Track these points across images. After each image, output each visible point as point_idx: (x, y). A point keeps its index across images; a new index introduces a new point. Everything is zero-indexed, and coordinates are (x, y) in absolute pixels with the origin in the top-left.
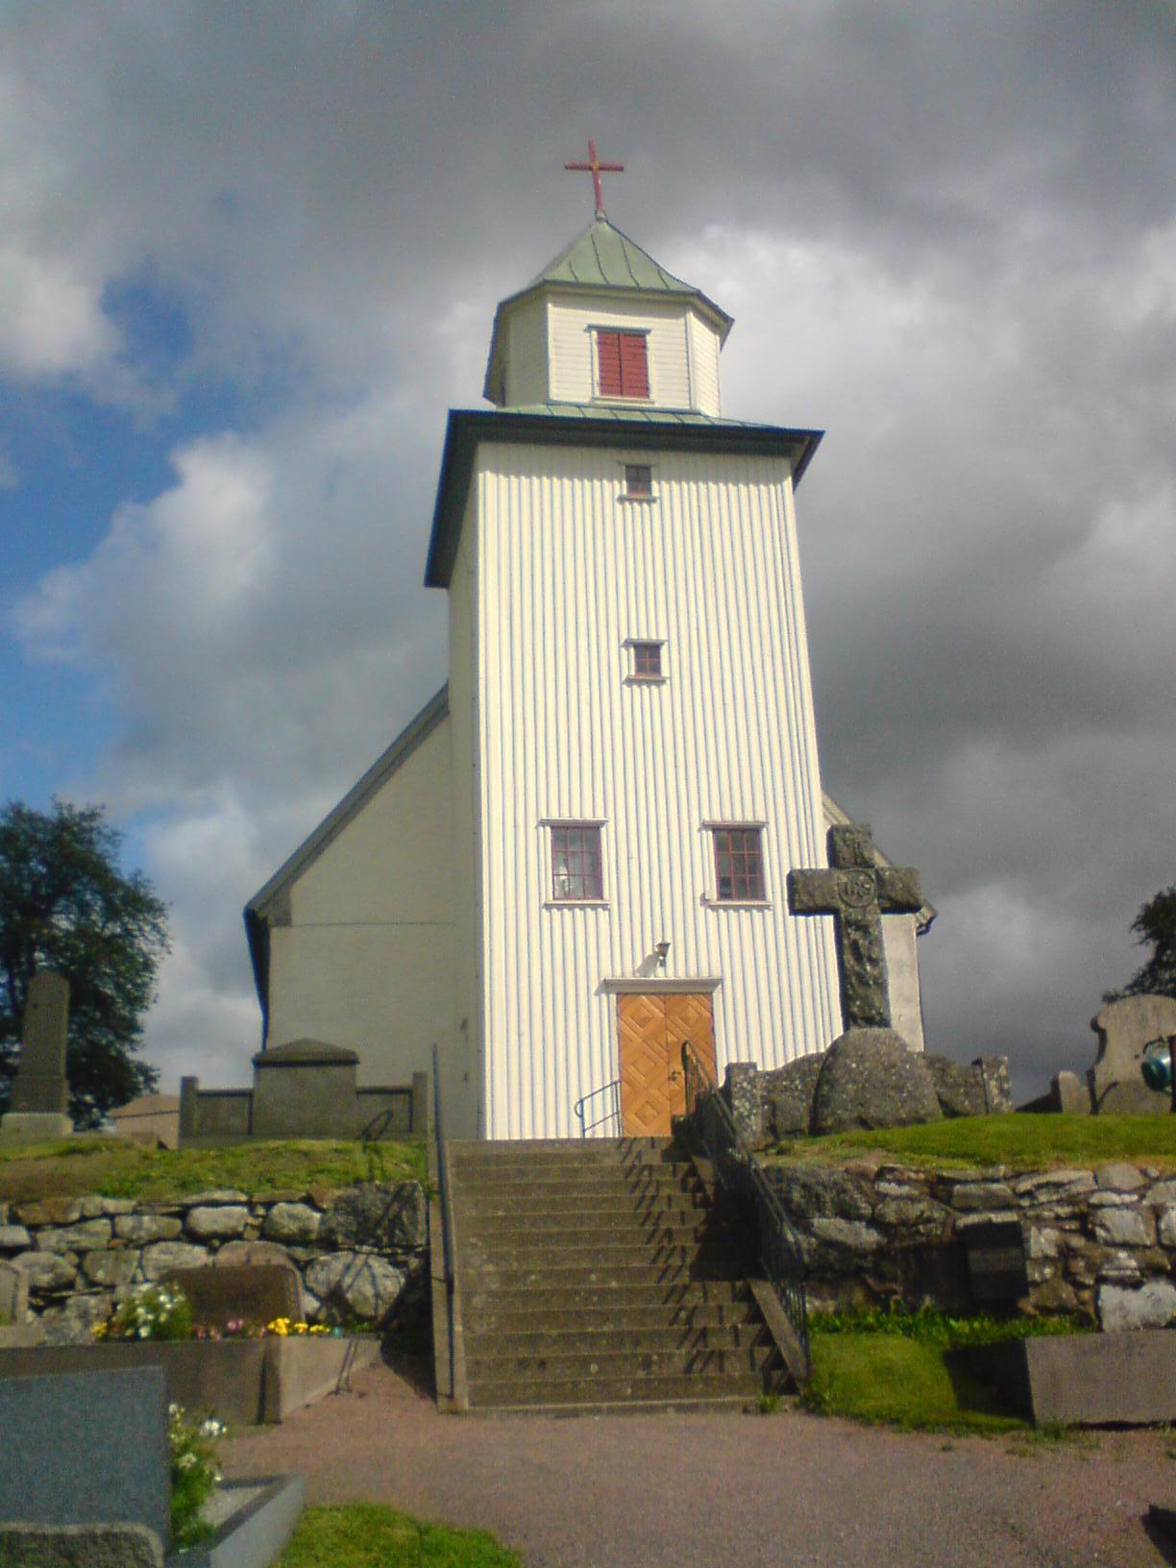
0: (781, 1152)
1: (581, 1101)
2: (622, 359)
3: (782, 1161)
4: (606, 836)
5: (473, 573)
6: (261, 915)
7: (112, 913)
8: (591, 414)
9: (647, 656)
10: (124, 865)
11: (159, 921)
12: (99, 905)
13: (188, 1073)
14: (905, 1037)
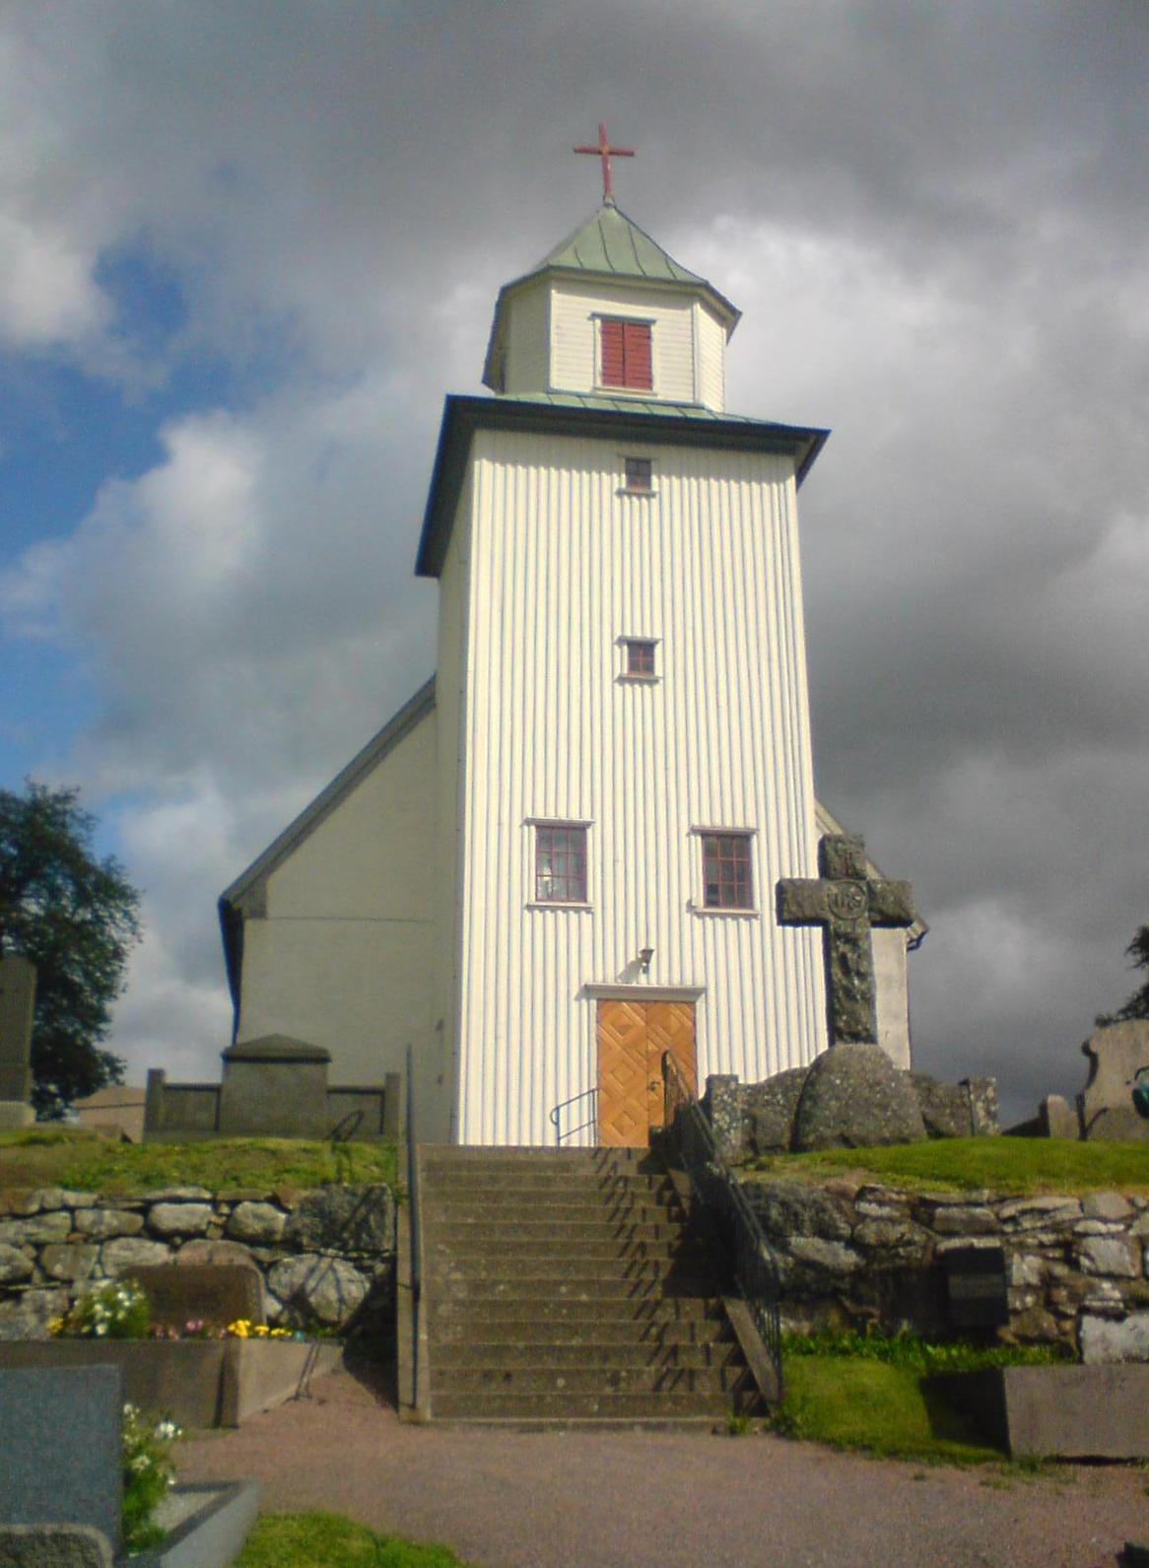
0: (761, 1168)
1: (557, 1109)
2: (626, 349)
3: (761, 1177)
4: (592, 837)
5: (465, 562)
6: (236, 906)
7: (83, 898)
8: (591, 404)
9: (641, 654)
10: (97, 851)
11: (131, 908)
12: (70, 889)
13: (155, 1065)
14: (892, 1054)
